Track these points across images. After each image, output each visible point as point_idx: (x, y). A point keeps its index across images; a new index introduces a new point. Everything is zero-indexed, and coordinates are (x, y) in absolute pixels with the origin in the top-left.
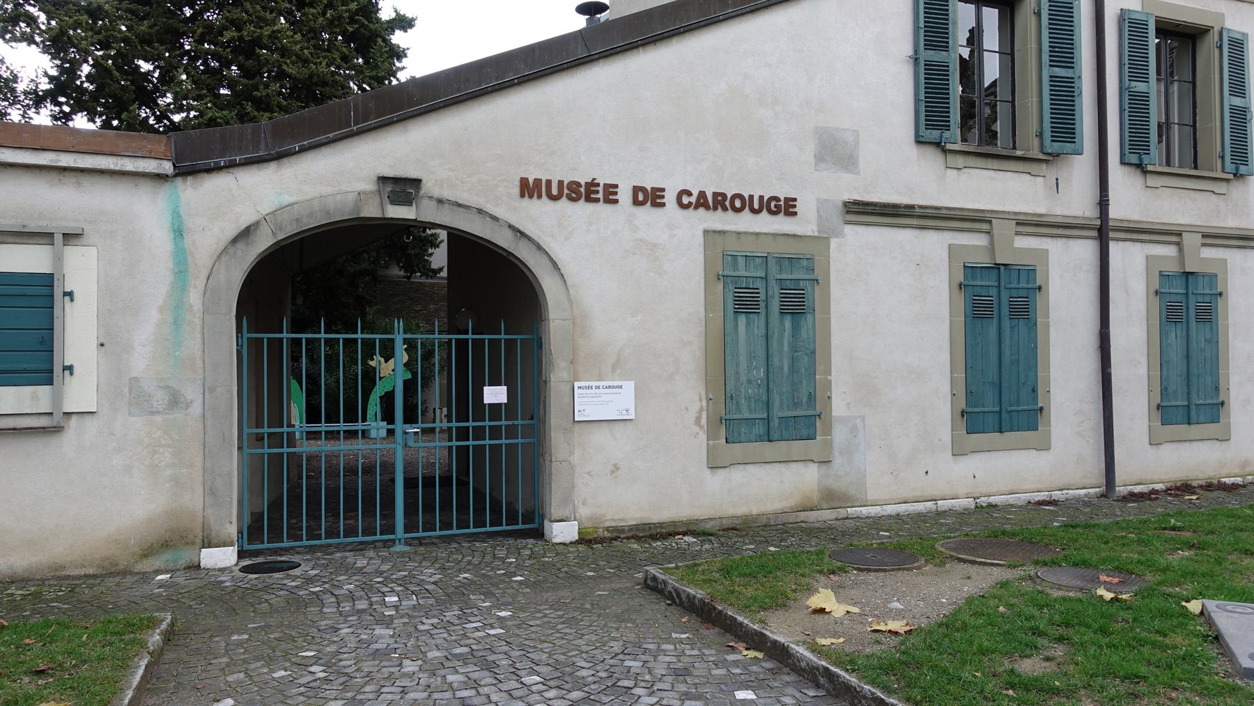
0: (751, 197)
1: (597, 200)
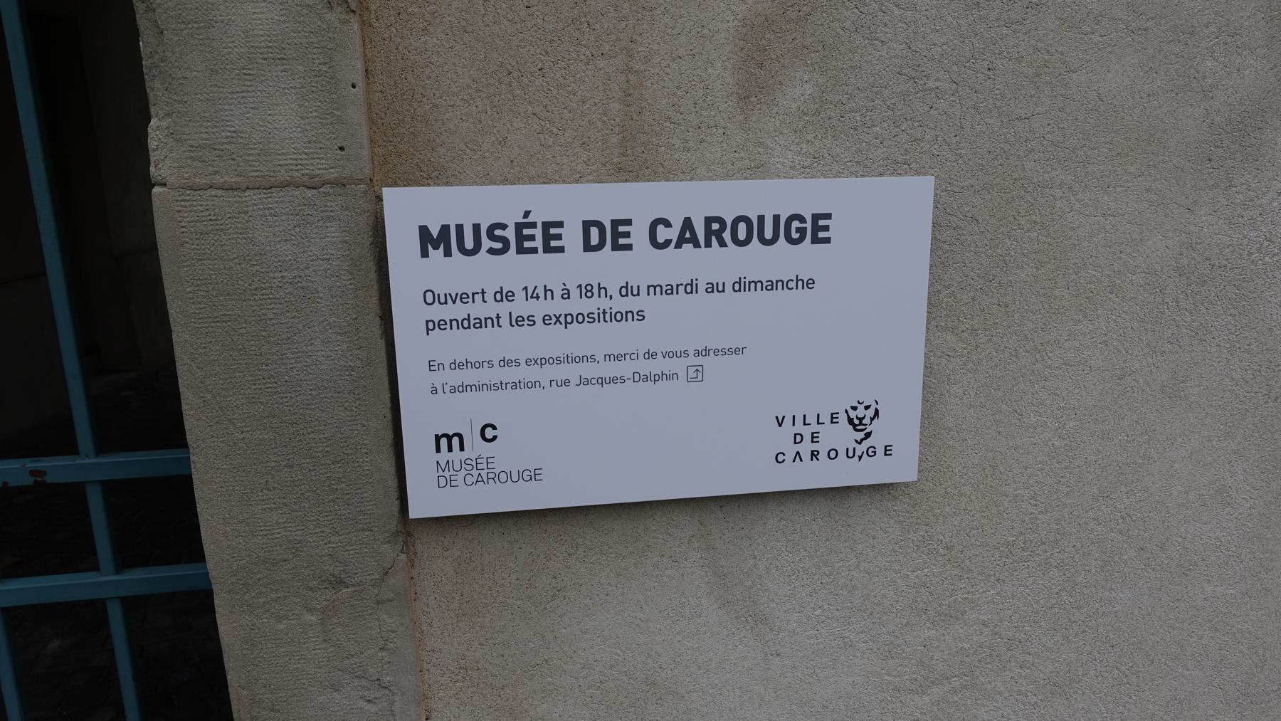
0: (761, 219)
1: (534, 251)
